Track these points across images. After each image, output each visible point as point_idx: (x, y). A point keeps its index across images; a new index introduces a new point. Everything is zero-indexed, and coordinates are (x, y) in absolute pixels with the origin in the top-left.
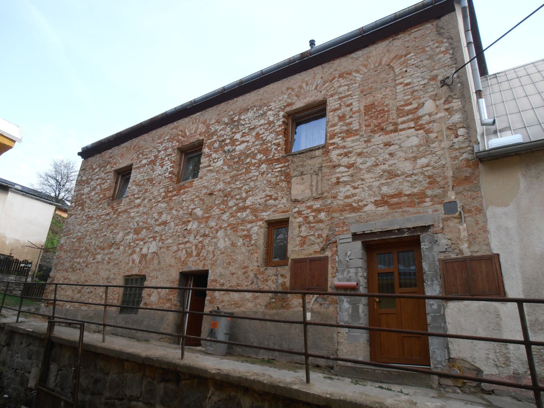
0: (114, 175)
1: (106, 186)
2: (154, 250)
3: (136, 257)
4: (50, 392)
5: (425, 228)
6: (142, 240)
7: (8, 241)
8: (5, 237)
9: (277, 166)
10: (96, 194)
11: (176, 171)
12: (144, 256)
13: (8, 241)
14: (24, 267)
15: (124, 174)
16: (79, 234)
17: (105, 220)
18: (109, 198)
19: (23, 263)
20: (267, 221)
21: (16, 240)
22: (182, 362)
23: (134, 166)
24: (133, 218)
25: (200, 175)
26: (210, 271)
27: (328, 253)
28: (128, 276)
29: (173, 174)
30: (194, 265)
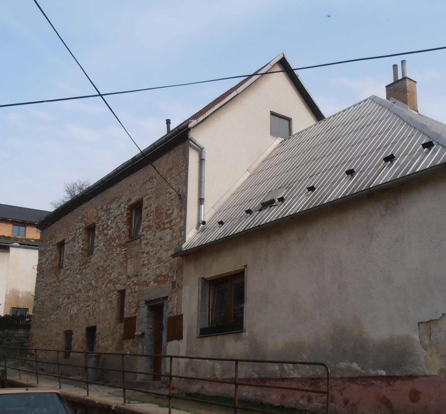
0: (58, 248)
1: (53, 257)
2: (75, 312)
3: (68, 317)
4: (222, 404)
5: (166, 298)
6: (71, 303)
7: (21, 295)
8: (18, 291)
9: (123, 250)
10: (49, 263)
11: (86, 247)
12: (71, 316)
13: (21, 295)
14: (29, 321)
15: (137, 208)
16: (42, 298)
17: (54, 287)
18: (56, 267)
19: (27, 318)
20: (118, 291)
21: (28, 292)
22: (88, 398)
23: (66, 242)
24: (66, 286)
25: (94, 254)
26: (97, 327)
27: (137, 314)
28: (65, 331)
29: (84, 250)
30: (92, 324)
